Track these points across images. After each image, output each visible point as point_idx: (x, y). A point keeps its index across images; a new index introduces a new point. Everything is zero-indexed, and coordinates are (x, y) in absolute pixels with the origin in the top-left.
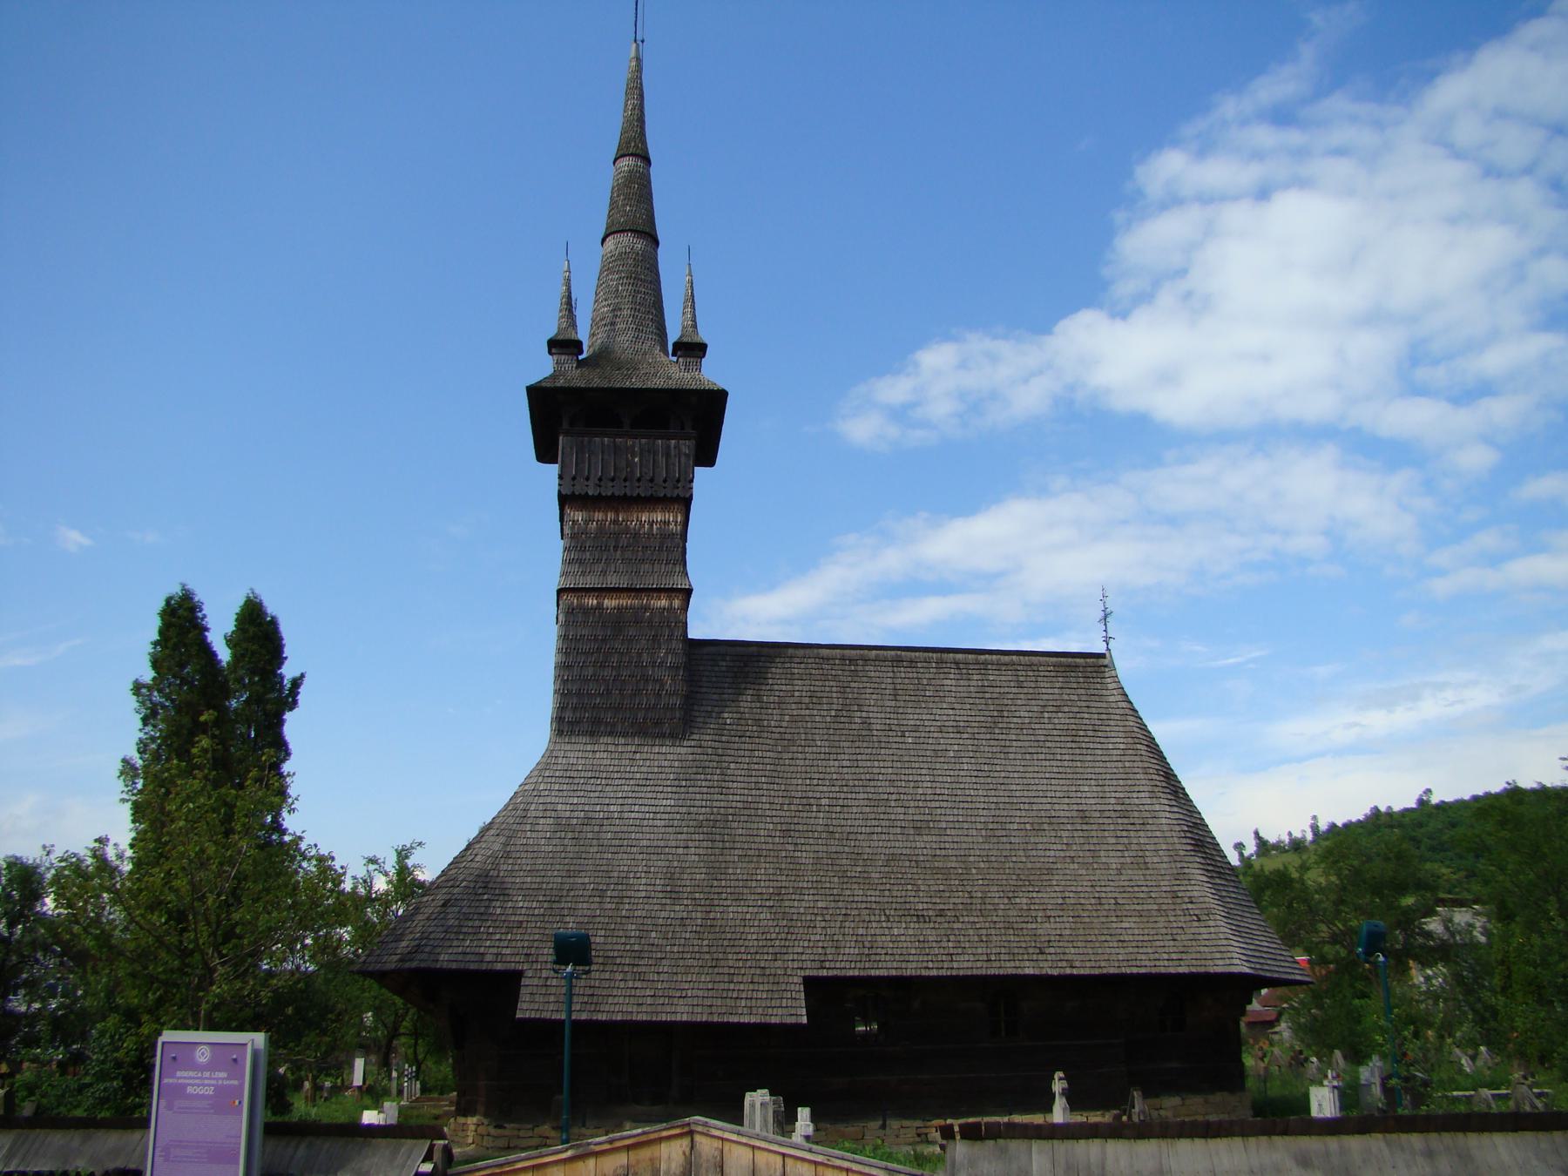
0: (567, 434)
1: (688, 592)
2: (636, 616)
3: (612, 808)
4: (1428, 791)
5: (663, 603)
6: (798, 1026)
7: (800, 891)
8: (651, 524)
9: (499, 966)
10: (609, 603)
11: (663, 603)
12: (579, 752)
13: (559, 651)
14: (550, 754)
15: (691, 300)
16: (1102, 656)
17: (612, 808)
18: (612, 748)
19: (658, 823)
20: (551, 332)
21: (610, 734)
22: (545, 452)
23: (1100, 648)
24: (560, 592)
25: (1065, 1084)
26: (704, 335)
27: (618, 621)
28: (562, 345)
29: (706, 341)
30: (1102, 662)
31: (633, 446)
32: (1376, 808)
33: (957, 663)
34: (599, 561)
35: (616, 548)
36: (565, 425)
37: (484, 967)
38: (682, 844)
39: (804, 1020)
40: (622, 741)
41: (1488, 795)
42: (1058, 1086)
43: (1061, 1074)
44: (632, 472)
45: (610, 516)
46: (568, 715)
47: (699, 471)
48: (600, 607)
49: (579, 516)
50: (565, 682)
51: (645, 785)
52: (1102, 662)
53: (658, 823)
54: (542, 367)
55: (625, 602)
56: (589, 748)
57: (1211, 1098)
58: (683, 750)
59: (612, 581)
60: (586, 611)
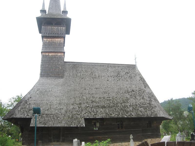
0: (43, 26)
1: (64, 53)
2: (55, 57)
3: (50, 89)
4: (172, 98)
5: (60, 54)
6: (83, 127)
7: (84, 103)
8: (58, 41)
9: (27, 117)
10: (50, 54)
11: (60, 54)
12: (45, 80)
13: (41, 62)
14: (39, 80)
15: (65, 5)
16: (135, 65)
17: (50, 89)
18: (50, 79)
19: (58, 92)
20: (41, 9)
21: (50, 77)
22: (40, 32)
23: (134, 64)
24: (42, 52)
25: (132, 137)
26: (67, 10)
27: (52, 58)
28: (43, 11)
29: (67, 11)
30: (135, 66)
31: (55, 28)
32: (165, 101)
33: (111, 66)
34: (49, 47)
35: (52, 45)
36: (43, 24)
37: (25, 117)
38: (62, 95)
39: (84, 126)
40: (52, 78)
41: (180, 99)
42: (131, 137)
43: (132, 135)
44: (54, 32)
45: (51, 40)
46: (43, 73)
47: (66, 35)
48: (49, 55)
49: (45, 40)
50: (42, 68)
51: (56, 87)
52: (135, 66)
53: (58, 92)
54: (39, 15)
55: (53, 54)
56: (46, 79)
57: (156, 139)
58: (63, 80)
59: (51, 51)
60: (46, 56)
